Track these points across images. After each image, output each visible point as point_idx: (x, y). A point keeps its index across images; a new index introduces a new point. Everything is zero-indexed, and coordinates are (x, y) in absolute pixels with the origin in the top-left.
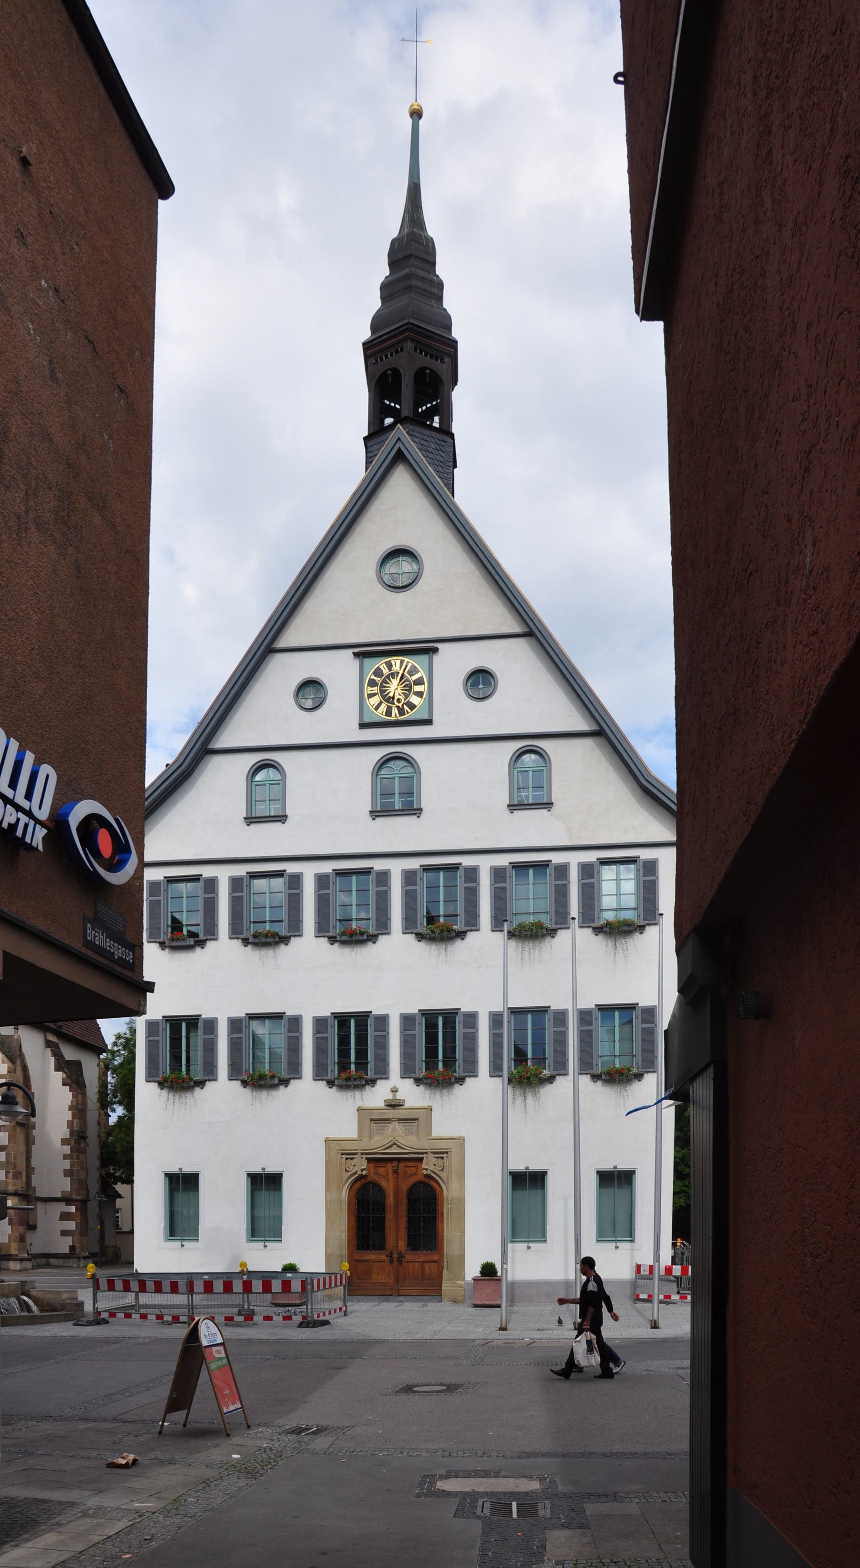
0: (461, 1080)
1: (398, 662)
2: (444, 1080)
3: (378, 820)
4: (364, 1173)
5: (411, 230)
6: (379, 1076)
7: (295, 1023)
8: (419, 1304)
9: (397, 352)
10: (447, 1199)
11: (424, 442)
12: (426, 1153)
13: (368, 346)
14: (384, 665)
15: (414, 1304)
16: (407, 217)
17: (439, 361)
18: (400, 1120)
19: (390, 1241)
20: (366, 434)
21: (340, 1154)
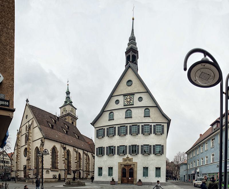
7: (126, 146)
18: (128, 160)
19: (127, 176)
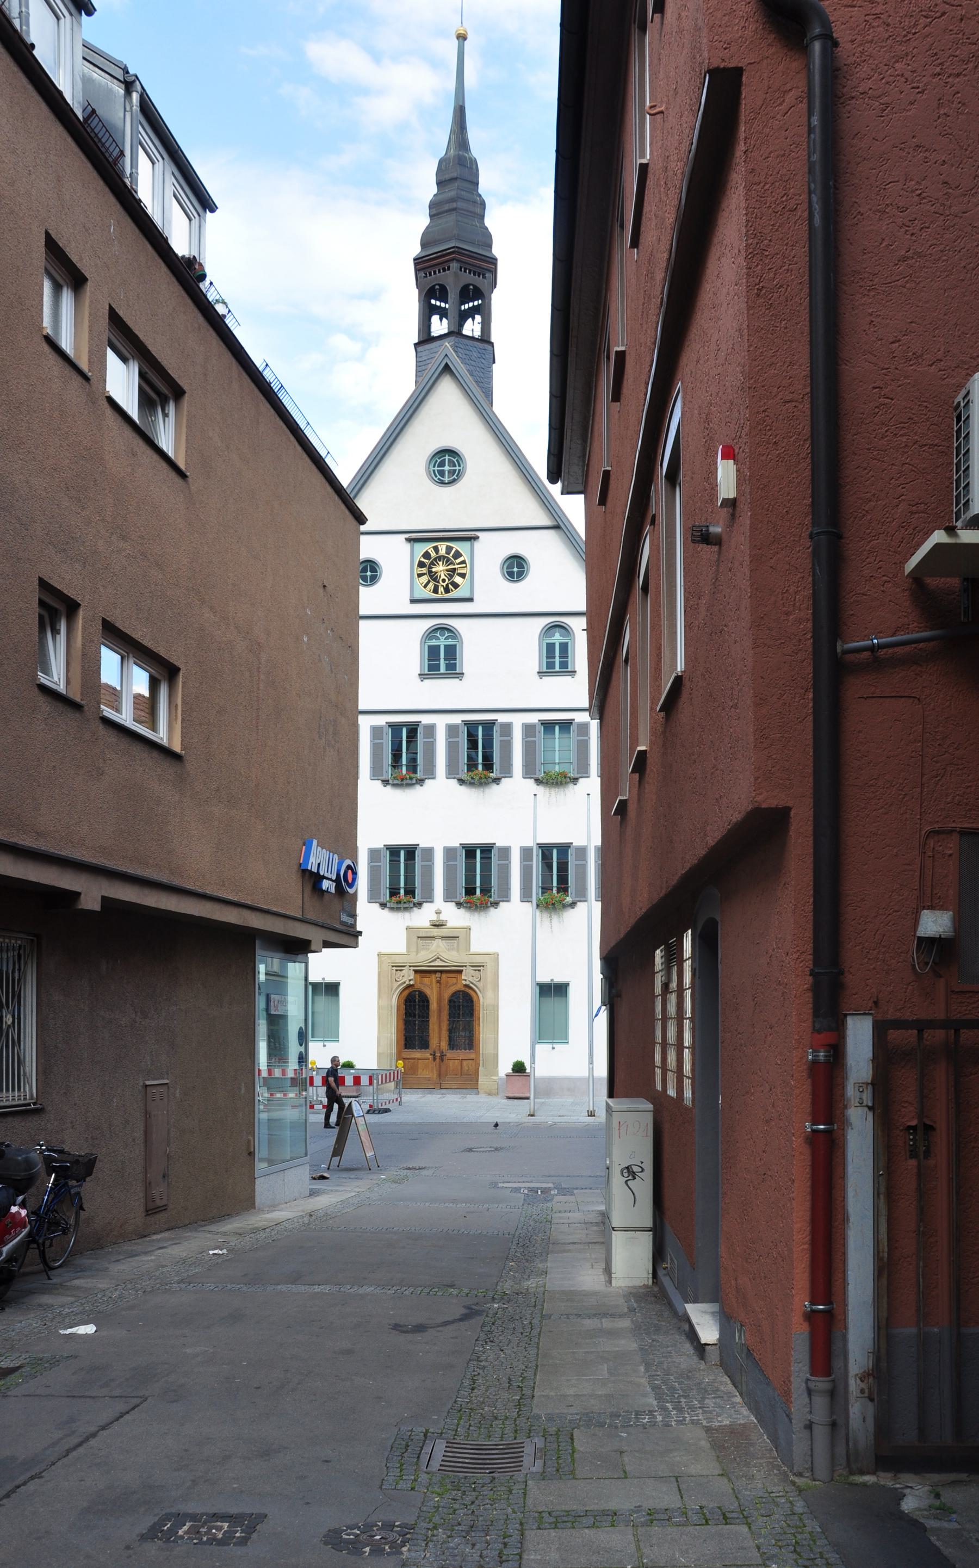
0: (496, 904)
1: (444, 548)
2: (481, 904)
3: (426, 681)
4: (412, 983)
5: (457, 153)
6: (425, 900)
8: (459, 1096)
9: (444, 270)
10: (483, 1005)
11: (467, 352)
12: (466, 966)
13: (417, 261)
14: (432, 549)
15: (455, 1096)
16: (453, 137)
17: (481, 276)
19: (434, 1042)
20: (416, 341)
21: (390, 967)
